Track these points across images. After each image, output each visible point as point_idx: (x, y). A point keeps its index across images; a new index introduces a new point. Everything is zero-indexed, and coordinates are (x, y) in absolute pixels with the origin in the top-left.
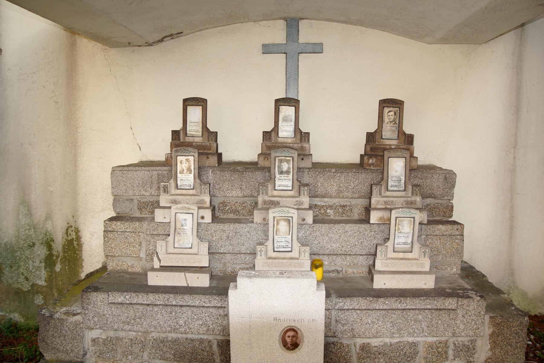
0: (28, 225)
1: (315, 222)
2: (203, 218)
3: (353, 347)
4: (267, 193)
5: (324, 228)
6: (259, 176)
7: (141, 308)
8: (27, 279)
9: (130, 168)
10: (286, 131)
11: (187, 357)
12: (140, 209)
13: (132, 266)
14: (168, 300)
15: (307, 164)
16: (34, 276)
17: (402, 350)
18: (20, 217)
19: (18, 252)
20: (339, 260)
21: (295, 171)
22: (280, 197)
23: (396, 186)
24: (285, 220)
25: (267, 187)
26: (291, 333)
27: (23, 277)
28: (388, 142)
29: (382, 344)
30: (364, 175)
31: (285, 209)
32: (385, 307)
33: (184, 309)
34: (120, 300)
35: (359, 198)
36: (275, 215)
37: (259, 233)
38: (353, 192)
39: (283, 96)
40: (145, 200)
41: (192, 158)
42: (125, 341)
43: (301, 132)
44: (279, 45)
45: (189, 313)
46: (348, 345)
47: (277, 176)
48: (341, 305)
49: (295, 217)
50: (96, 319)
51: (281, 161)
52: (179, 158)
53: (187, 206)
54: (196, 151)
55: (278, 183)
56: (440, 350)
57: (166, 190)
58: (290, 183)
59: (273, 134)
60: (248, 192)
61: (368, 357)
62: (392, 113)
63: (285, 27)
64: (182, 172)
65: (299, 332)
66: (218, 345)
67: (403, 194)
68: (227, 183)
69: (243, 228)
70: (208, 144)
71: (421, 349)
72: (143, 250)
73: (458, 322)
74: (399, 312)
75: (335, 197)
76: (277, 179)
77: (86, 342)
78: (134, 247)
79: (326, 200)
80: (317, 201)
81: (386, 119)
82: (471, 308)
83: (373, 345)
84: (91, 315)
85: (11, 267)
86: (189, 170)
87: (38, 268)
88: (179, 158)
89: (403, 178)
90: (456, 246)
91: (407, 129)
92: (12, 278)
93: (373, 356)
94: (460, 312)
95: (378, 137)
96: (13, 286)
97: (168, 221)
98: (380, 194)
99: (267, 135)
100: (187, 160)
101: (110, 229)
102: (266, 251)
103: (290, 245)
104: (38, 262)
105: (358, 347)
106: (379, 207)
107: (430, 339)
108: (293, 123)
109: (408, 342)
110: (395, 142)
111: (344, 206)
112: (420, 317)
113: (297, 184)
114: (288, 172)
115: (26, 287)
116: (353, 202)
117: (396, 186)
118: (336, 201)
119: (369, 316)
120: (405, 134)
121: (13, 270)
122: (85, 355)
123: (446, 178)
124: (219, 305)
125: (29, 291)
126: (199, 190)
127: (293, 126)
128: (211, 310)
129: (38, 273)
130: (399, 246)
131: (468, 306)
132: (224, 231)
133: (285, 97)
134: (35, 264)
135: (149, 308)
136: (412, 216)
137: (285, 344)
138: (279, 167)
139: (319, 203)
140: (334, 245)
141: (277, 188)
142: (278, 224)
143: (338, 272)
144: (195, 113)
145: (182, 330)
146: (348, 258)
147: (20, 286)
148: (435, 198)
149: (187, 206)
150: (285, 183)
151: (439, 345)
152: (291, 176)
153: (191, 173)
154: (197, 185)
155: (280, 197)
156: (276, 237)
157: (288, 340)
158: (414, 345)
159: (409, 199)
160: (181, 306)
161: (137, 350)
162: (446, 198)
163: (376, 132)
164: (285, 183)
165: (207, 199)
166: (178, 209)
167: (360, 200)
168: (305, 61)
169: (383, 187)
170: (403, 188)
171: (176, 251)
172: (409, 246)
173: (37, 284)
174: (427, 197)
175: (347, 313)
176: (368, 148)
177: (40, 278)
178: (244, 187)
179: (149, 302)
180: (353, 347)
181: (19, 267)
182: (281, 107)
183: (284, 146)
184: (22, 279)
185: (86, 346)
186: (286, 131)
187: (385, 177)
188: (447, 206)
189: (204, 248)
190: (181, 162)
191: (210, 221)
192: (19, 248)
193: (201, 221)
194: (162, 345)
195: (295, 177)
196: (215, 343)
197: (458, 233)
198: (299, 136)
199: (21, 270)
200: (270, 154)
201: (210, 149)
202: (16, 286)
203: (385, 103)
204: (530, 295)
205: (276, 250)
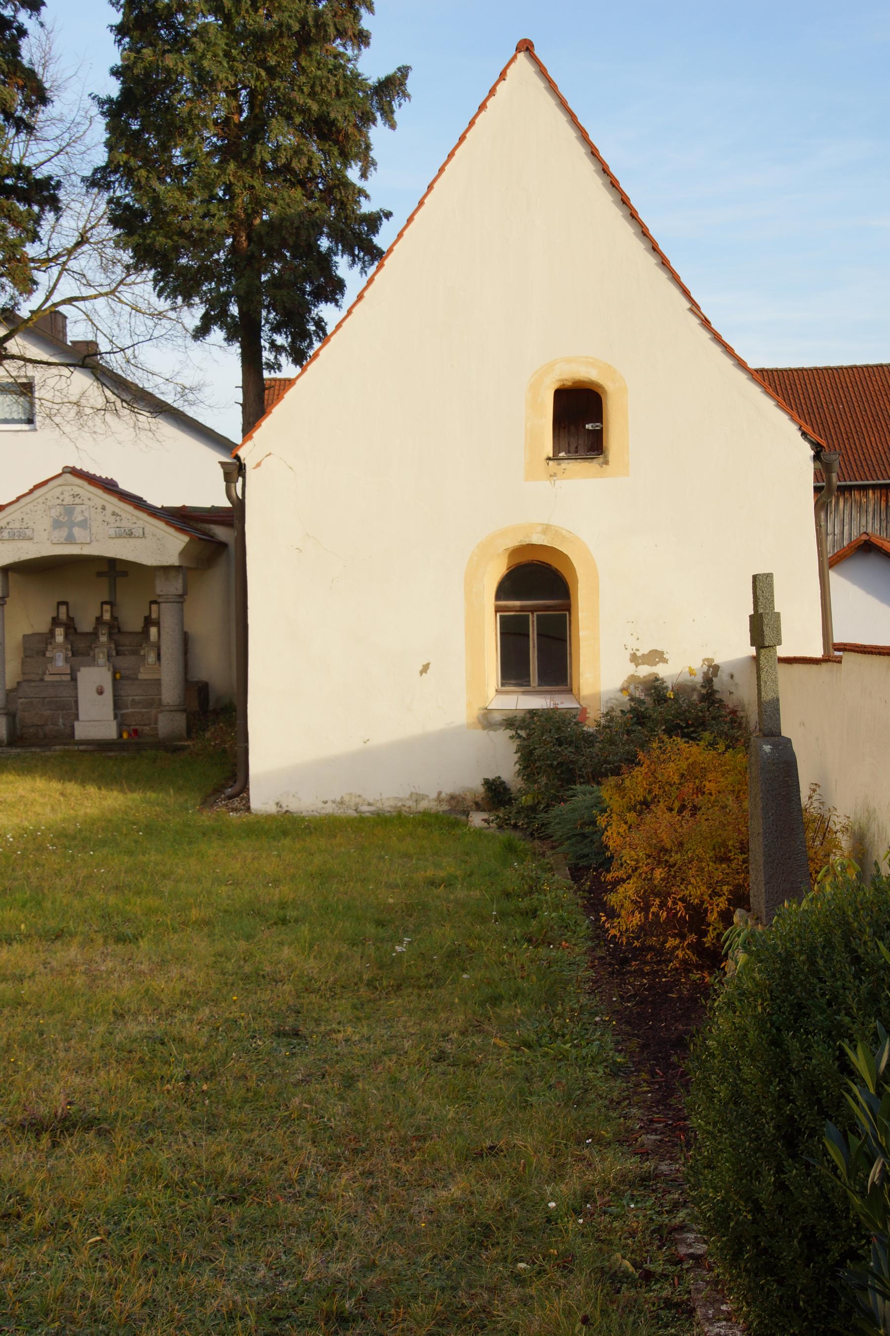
57: (51, 643)
165: (69, 647)
189: (68, 666)
203: (60, 604)
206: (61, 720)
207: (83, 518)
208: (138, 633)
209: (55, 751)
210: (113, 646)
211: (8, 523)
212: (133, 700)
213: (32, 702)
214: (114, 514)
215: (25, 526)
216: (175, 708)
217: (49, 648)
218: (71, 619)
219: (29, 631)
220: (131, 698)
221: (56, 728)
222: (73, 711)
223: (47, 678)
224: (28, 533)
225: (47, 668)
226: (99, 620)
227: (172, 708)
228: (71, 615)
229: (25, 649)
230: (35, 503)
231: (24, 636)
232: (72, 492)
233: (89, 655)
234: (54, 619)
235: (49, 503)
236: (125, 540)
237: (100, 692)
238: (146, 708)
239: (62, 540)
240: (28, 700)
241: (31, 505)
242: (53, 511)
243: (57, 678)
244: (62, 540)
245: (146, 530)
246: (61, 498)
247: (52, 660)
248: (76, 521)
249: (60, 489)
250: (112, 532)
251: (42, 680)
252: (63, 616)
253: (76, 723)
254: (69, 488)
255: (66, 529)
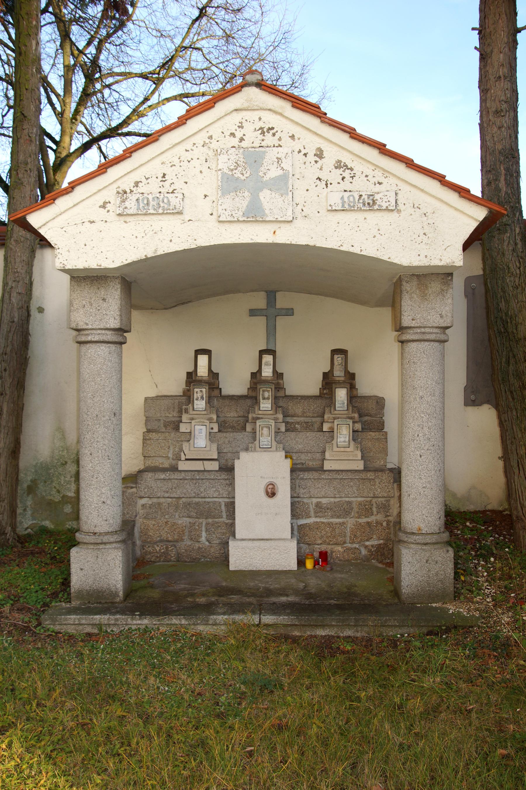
0: (62, 447)
1: (287, 430)
2: (212, 429)
3: (311, 505)
4: (254, 413)
5: (293, 435)
6: (249, 402)
7: (176, 481)
8: (58, 491)
9: (163, 398)
10: (267, 372)
11: (205, 514)
12: (165, 426)
13: (162, 463)
14: (194, 476)
15: (280, 394)
16: (65, 489)
17: (342, 506)
18: (56, 441)
19: (52, 470)
20: (303, 457)
21: (273, 398)
22: (264, 415)
23: (341, 407)
24: (267, 427)
25: (254, 408)
26: (271, 486)
27: (55, 490)
28: (337, 379)
29: (328, 502)
30: (320, 401)
31: (266, 420)
32: (330, 478)
33: (204, 481)
34: (162, 477)
35: (317, 417)
36: (260, 424)
37: (250, 438)
38: (313, 413)
39: (264, 348)
40: (169, 420)
41: (204, 390)
42: (164, 504)
43: (277, 372)
44: (262, 310)
45: (207, 483)
46: (307, 504)
47: (261, 401)
48: (302, 476)
49: (273, 425)
50: (146, 490)
51: (264, 391)
52: (196, 390)
53: (202, 420)
54: (207, 385)
55: (262, 405)
56: (367, 507)
57: (186, 411)
58: (270, 406)
59: (258, 374)
60: (241, 414)
61: (321, 511)
62: (340, 359)
63: (265, 297)
64: (197, 399)
65: (276, 486)
66: (225, 505)
67: (346, 412)
68: (227, 407)
69: (239, 436)
70: (213, 381)
71: (354, 506)
72: (171, 452)
73: (376, 487)
74: (338, 481)
75: (301, 417)
76: (261, 403)
77: (138, 507)
78: (164, 449)
79: (295, 418)
80: (289, 419)
81: (336, 363)
82: (384, 478)
83: (323, 502)
84: (143, 488)
85: (45, 482)
86: (202, 398)
87: (69, 482)
88: (196, 390)
89: (346, 402)
90: (382, 446)
91: (351, 370)
92: (45, 491)
93: (324, 510)
94: (377, 481)
95: (330, 375)
96: (46, 498)
97: (189, 431)
98: (331, 412)
99: (253, 375)
100: (201, 391)
101: (147, 438)
102: (255, 447)
103: (270, 444)
104: (69, 477)
105: (314, 504)
106: (329, 421)
107: (360, 499)
108: (272, 367)
109: (346, 501)
110: (343, 379)
111: (307, 422)
112: (352, 484)
113: (274, 406)
114: (268, 398)
115: (57, 498)
116: (314, 420)
117: (341, 407)
118: (302, 419)
119: (320, 483)
120: (349, 372)
121: (46, 484)
122: (136, 516)
123: (377, 402)
124: (226, 478)
125: (60, 502)
126: (209, 411)
127: (272, 369)
128: (221, 481)
129: (68, 486)
130: (340, 443)
131: (382, 476)
132: (226, 438)
133: (266, 348)
134: (66, 479)
135: (181, 481)
136: (348, 423)
137: (267, 493)
138: (263, 395)
139: (290, 421)
140: (300, 446)
141: (261, 409)
142: (262, 429)
143: (303, 464)
144: (203, 360)
145: (202, 495)
146: (309, 454)
147: (52, 498)
148: (371, 416)
149: (202, 420)
150: (266, 405)
151: (366, 503)
152: (270, 401)
153: (203, 400)
154: (208, 408)
155: (264, 415)
156: (261, 438)
157: (269, 491)
158: (349, 503)
159: (350, 416)
160: (202, 479)
161: (172, 511)
162: (378, 416)
163: (329, 372)
164: (266, 405)
165: (215, 417)
166: (196, 422)
167: (318, 418)
168: (281, 321)
169: (332, 408)
170: (346, 409)
171: (195, 449)
172: (347, 443)
173: (67, 496)
174: (365, 416)
175: (306, 481)
176: (324, 383)
177: (70, 491)
178: (238, 410)
179: (181, 478)
180: (311, 505)
181: (52, 482)
182: (264, 356)
183: (266, 382)
184: (54, 492)
185: (137, 510)
186: (267, 372)
187: (334, 402)
188: (380, 422)
189: (214, 447)
190: (197, 392)
191: (217, 431)
192: (53, 466)
193: (211, 431)
194: (188, 506)
195: (273, 401)
196: (223, 504)
197: (383, 437)
198: (276, 376)
199: (54, 484)
200: (256, 388)
201: (214, 385)
202: (49, 498)
203: (335, 352)
204: (459, 495)
205: (261, 447)
206: (204, 534)
207: (280, 172)
208: (316, 397)
209: (215, 624)
210: (280, 416)
211: (137, 184)
212: (318, 505)
213: (159, 504)
214: (339, 165)
215: (167, 187)
216: (434, 539)
217: (185, 418)
218: (214, 375)
219: (152, 393)
220: (315, 501)
221: (197, 545)
222: (224, 519)
223: (183, 466)
224: (174, 200)
225: (181, 450)
226: (256, 376)
227: (428, 539)
228: (214, 370)
229: (148, 420)
230: (188, 145)
231: (146, 399)
232: (261, 124)
233: (244, 428)
234: (189, 375)
235: (214, 145)
236: (360, 216)
237: (271, 493)
238: (338, 517)
239: (239, 215)
240: (155, 500)
241: (180, 150)
242: (223, 158)
243: (198, 466)
244: (239, 215)
245: (400, 197)
246: (239, 135)
247: (189, 436)
248: (266, 178)
249: (237, 117)
250: (335, 199)
251: (174, 469)
252: (203, 371)
253: (231, 543)
254: (255, 115)
255: (246, 194)
